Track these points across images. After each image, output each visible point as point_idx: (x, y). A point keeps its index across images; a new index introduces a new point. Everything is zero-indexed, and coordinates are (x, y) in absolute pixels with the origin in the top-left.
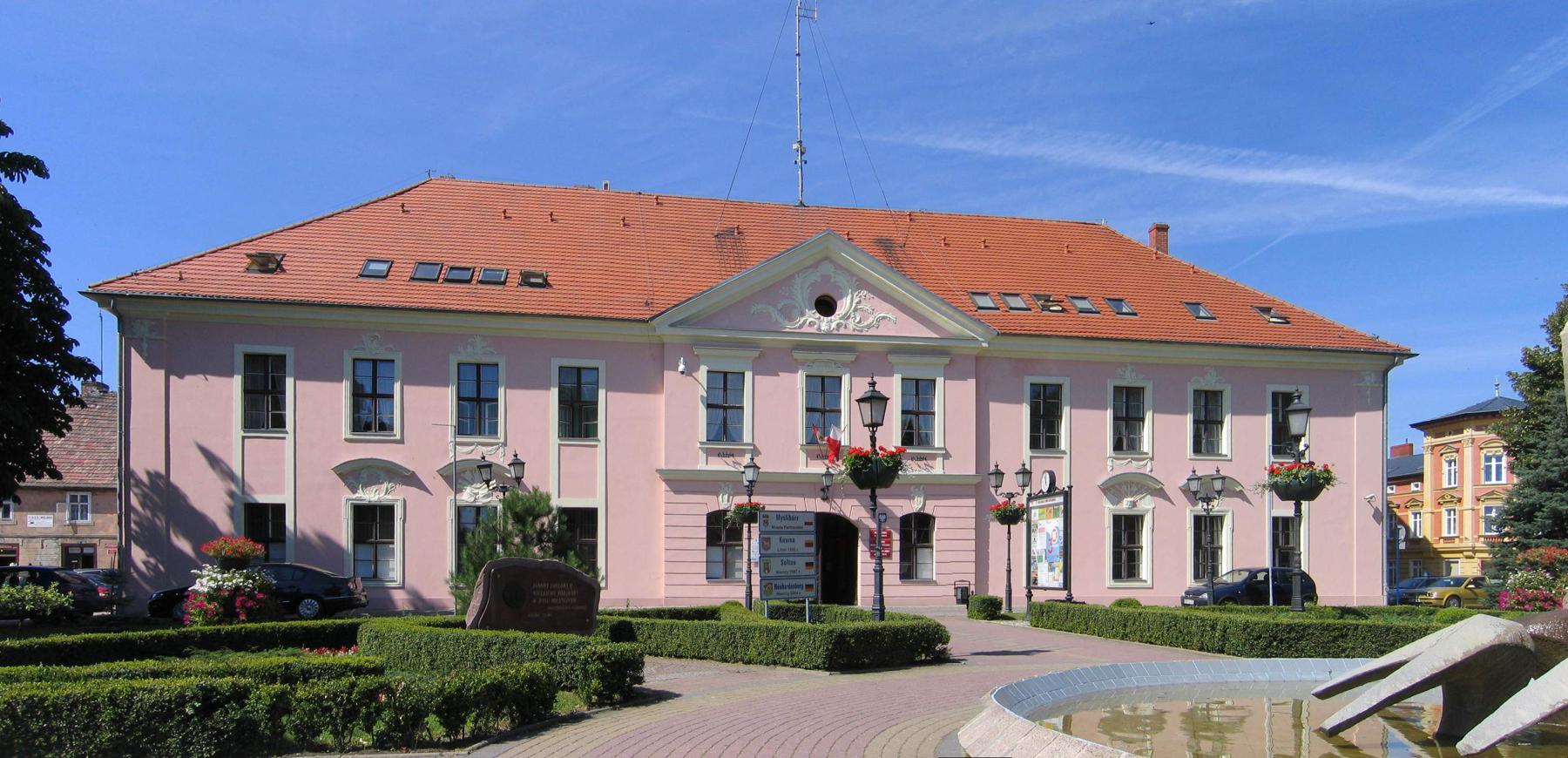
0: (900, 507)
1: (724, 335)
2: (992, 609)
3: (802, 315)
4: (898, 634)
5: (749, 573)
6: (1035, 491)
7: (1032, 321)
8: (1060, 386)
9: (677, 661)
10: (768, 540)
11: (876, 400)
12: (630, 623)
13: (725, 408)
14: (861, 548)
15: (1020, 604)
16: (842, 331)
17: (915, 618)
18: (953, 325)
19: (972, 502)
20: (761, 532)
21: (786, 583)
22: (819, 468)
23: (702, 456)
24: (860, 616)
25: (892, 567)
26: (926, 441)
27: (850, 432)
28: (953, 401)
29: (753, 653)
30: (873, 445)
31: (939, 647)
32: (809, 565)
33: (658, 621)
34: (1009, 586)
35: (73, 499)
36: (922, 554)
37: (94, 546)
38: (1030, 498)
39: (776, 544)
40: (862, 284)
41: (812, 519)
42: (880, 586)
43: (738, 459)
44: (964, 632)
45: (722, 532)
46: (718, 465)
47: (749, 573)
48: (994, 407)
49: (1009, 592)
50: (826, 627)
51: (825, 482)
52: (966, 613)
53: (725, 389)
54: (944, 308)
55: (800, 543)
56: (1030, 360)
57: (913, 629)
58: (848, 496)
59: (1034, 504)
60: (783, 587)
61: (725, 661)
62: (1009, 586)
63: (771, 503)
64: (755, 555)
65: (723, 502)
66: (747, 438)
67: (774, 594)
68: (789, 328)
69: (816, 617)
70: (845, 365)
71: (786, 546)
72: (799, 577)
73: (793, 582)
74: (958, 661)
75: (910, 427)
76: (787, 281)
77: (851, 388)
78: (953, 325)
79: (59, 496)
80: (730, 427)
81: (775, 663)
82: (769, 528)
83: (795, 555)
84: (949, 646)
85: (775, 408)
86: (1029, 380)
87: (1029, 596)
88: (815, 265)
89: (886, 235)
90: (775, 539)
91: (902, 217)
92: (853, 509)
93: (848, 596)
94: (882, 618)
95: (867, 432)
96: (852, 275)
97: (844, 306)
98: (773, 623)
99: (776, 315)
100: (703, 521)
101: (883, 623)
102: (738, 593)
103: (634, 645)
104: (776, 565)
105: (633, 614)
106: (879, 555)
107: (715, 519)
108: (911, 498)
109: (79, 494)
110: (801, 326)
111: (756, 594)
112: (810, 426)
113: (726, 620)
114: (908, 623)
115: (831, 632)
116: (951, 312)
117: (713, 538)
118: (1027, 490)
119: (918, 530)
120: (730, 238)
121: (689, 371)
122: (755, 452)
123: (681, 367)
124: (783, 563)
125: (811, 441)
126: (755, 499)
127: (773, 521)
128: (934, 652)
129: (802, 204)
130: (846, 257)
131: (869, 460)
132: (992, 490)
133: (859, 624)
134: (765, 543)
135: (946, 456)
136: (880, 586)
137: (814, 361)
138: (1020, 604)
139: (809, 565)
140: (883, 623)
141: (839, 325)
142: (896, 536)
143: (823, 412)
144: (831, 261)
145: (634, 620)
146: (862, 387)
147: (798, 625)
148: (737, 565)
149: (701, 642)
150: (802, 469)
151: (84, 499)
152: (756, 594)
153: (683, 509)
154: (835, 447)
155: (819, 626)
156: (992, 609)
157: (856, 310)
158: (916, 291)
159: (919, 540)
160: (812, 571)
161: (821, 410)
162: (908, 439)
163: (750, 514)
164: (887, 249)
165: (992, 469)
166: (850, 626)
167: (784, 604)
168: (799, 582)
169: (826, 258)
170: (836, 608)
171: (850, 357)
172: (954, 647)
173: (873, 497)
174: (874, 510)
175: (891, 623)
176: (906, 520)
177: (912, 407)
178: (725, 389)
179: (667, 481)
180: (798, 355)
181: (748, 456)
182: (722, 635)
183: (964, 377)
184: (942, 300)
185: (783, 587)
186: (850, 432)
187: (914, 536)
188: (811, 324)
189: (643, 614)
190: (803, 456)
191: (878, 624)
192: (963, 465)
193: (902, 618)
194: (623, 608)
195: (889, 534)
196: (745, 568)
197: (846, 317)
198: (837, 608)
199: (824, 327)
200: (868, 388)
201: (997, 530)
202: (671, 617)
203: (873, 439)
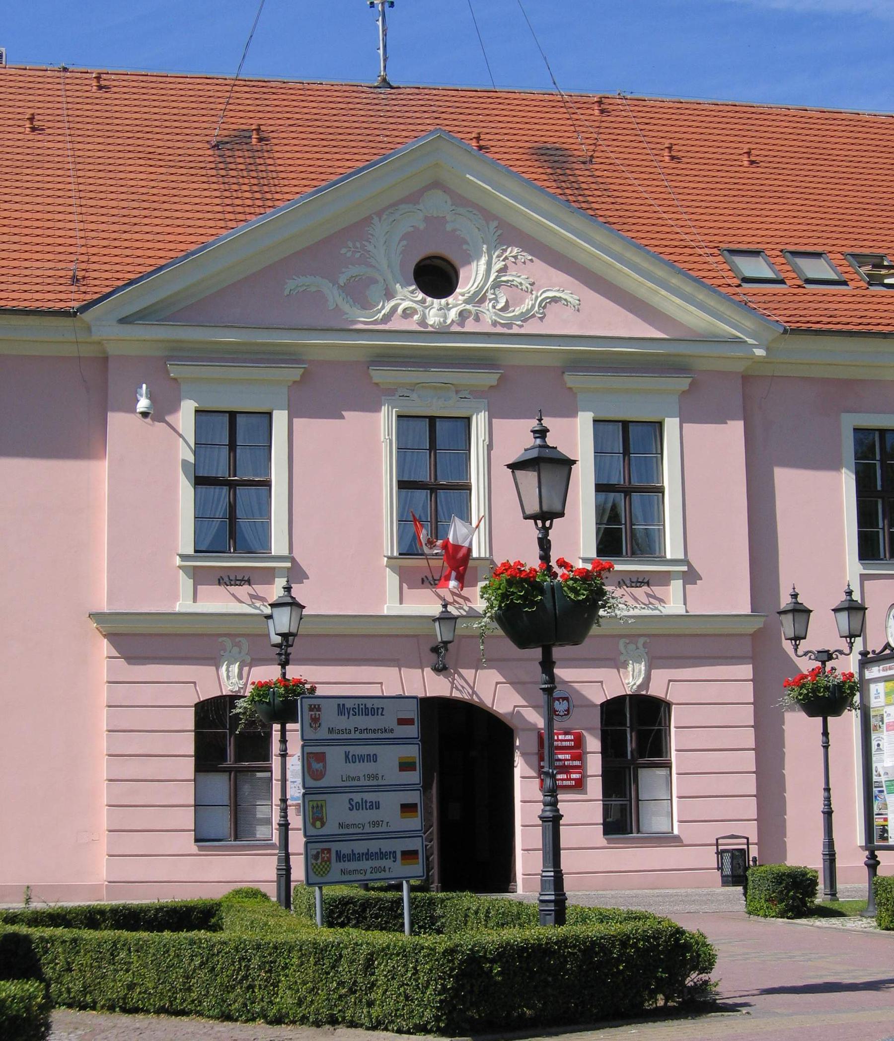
0: (597, 683)
1: (230, 337)
2: (795, 895)
3: (389, 295)
4: (592, 951)
5: (285, 827)
6: (875, 645)
7: (856, 303)
8: (856, 430)
9: (126, 1020)
10: (321, 758)
11: (548, 463)
12: (26, 940)
13: (232, 485)
14: (521, 768)
15: (853, 882)
16: (470, 326)
17: (632, 917)
18: (693, 314)
19: (746, 671)
20: (306, 742)
21: (360, 847)
22: (425, 605)
23: (185, 583)
24: (516, 916)
25: (584, 811)
26: (647, 546)
27: (494, 526)
28: (700, 467)
29: (286, 999)
30: (545, 557)
31: (692, 979)
32: (407, 808)
33: (88, 934)
34: (830, 844)
36: (649, 780)
38: (866, 660)
39: (337, 766)
40: (508, 234)
41: (412, 712)
42: (553, 851)
43: (260, 589)
44: (743, 945)
45: (227, 741)
46: (219, 602)
47: (285, 827)
49: (830, 858)
50: (442, 942)
51: (440, 633)
52: (741, 905)
53: (232, 446)
54: (675, 281)
55: (388, 759)
56: (849, 384)
57: (625, 941)
58: (493, 662)
59: (873, 672)
60: (353, 857)
61: (227, 1017)
62: (830, 844)
63: (329, 679)
64: (295, 791)
65: (229, 679)
66: (278, 545)
67: (336, 867)
68: (363, 320)
69: (426, 921)
70: (477, 393)
71: (360, 769)
73: (374, 846)
74: (733, 1008)
75: (614, 517)
76: (358, 230)
77: (493, 443)
78: (693, 314)
80: (243, 521)
81: (333, 1021)
82: (323, 733)
83: (378, 789)
84: (713, 976)
85: (334, 482)
86: (849, 422)
87: (873, 865)
88: (414, 198)
89: (553, 140)
90: (335, 754)
91: (583, 104)
92: (495, 690)
93: (500, 876)
94: (560, 919)
95: (532, 531)
96: (487, 215)
97: (472, 277)
98: (329, 935)
99: (334, 297)
100: (188, 720)
101: (562, 930)
102: (260, 870)
103: (31, 986)
104: (337, 811)
105: (37, 919)
106: (556, 781)
107: (212, 715)
108: (618, 664)
110: (387, 318)
111: (298, 872)
112: (407, 519)
113: (233, 931)
114: (614, 928)
115: (451, 952)
116: (688, 288)
117: (208, 757)
118: (858, 643)
119: (636, 732)
120: (242, 151)
121: (159, 412)
122: (296, 574)
123: (143, 404)
124: (354, 806)
125: (409, 549)
126: (294, 672)
127: (330, 718)
128: (682, 989)
129: (385, 83)
130: (477, 181)
131: (538, 588)
132: (788, 646)
133: (512, 935)
134: (313, 763)
135: (691, 576)
136: (553, 851)
137: (413, 387)
138: (853, 882)
139: (407, 808)
140: (562, 930)
141: (463, 316)
142: (593, 744)
143: (433, 489)
144: (446, 190)
145: (36, 933)
146: (517, 438)
147: (381, 938)
148: (261, 812)
149: (176, 978)
150: (390, 607)
152: (298, 872)
153: (146, 695)
154: (459, 562)
155: (427, 940)
156: (795, 895)
157: (497, 285)
158: (617, 248)
159: (642, 751)
160: (415, 823)
161: (431, 483)
162: (610, 543)
163: (283, 704)
164: (559, 169)
165: (785, 601)
166: (492, 937)
167: (356, 892)
168: (386, 846)
169: (437, 184)
170: (469, 900)
171: (489, 378)
172: (724, 979)
173: (547, 665)
174: (549, 692)
175: (579, 930)
176: (613, 709)
177: (616, 478)
178: (232, 446)
179: (113, 637)
180: (381, 376)
181: (281, 582)
182: (220, 961)
183: (721, 418)
184: (671, 265)
185: (353, 857)
186: (494, 526)
187: (631, 745)
188: (408, 314)
189: (58, 918)
190: (391, 580)
191: (550, 932)
192: (727, 595)
193: (603, 918)
194: (16, 905)
195: (579, 741)
196: (276, 819)
197: (478, 298)
198: (470, 900)
199: (433, 318)
200: (531, 441)
201: (800, 728)
202: (118, 926)
203: (544, 545)
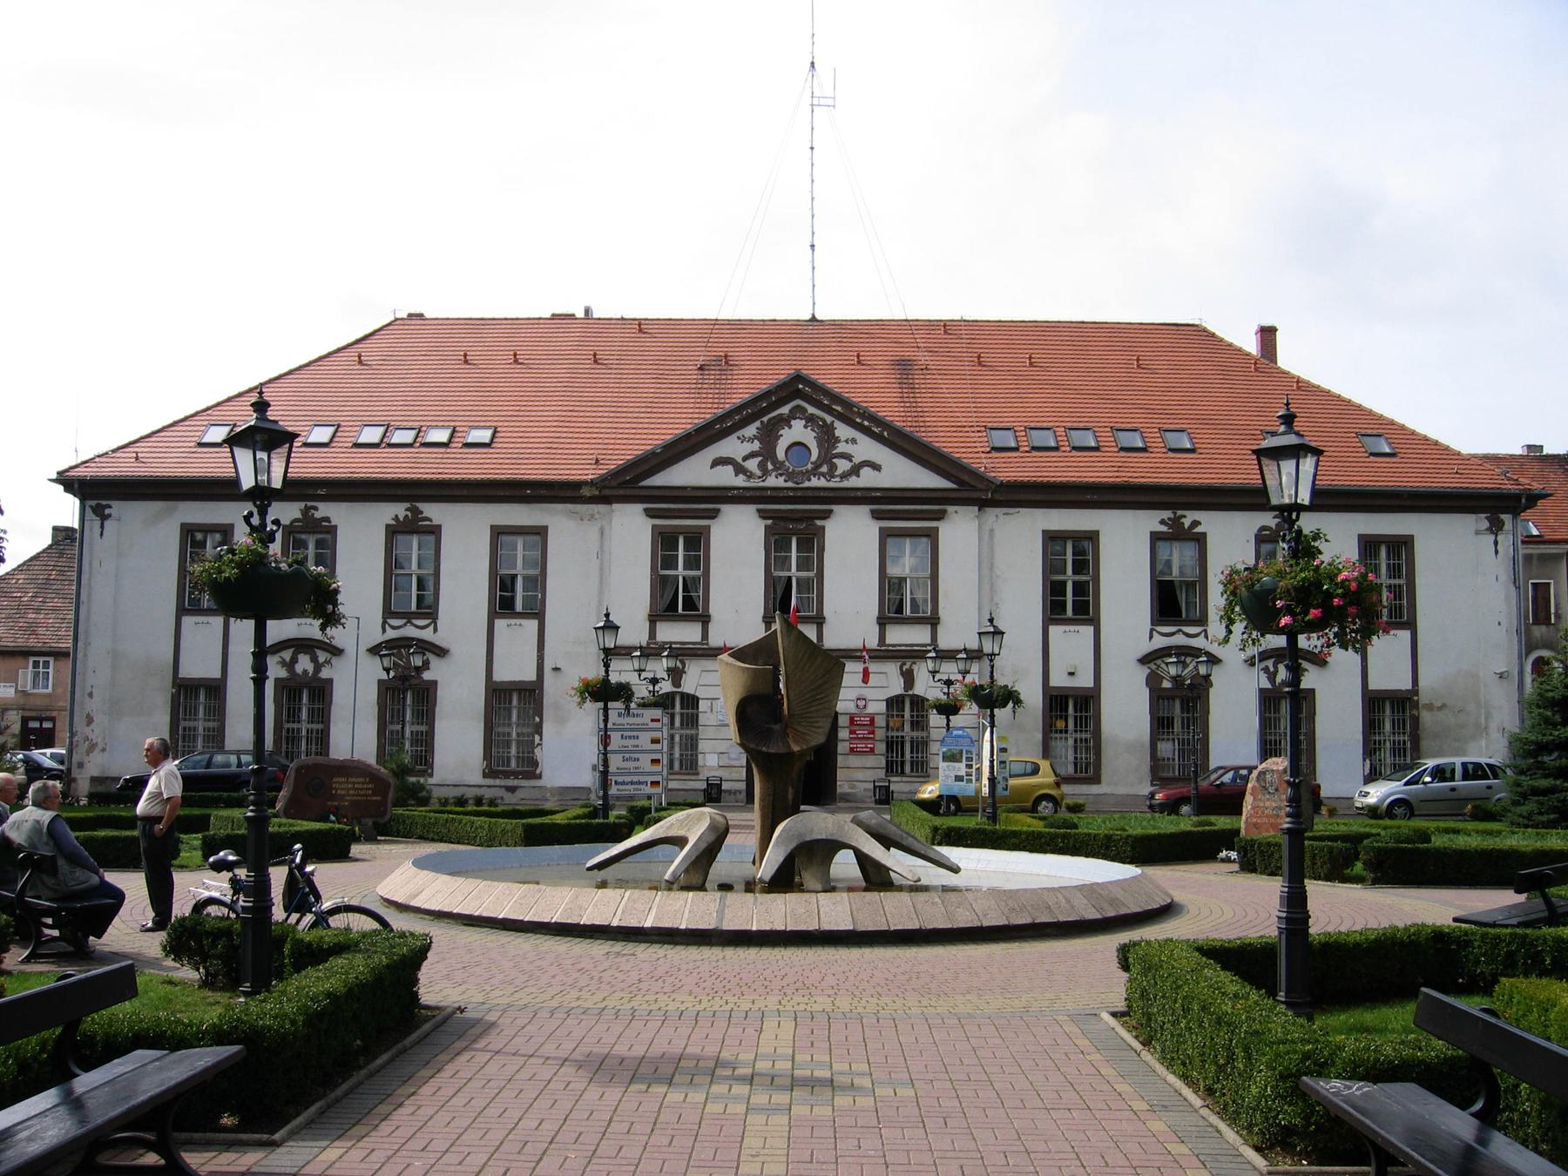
35: (36, 665)
37: (53, 719)
48: (534, 678)
60: (623, 783)
72: (642, 774)
73: (636, 779)
79: (20, 661)
109: (42, 659)
139: (655, 761)
151: (46, 665)
168: (642, 779)
185: (623, 783)
